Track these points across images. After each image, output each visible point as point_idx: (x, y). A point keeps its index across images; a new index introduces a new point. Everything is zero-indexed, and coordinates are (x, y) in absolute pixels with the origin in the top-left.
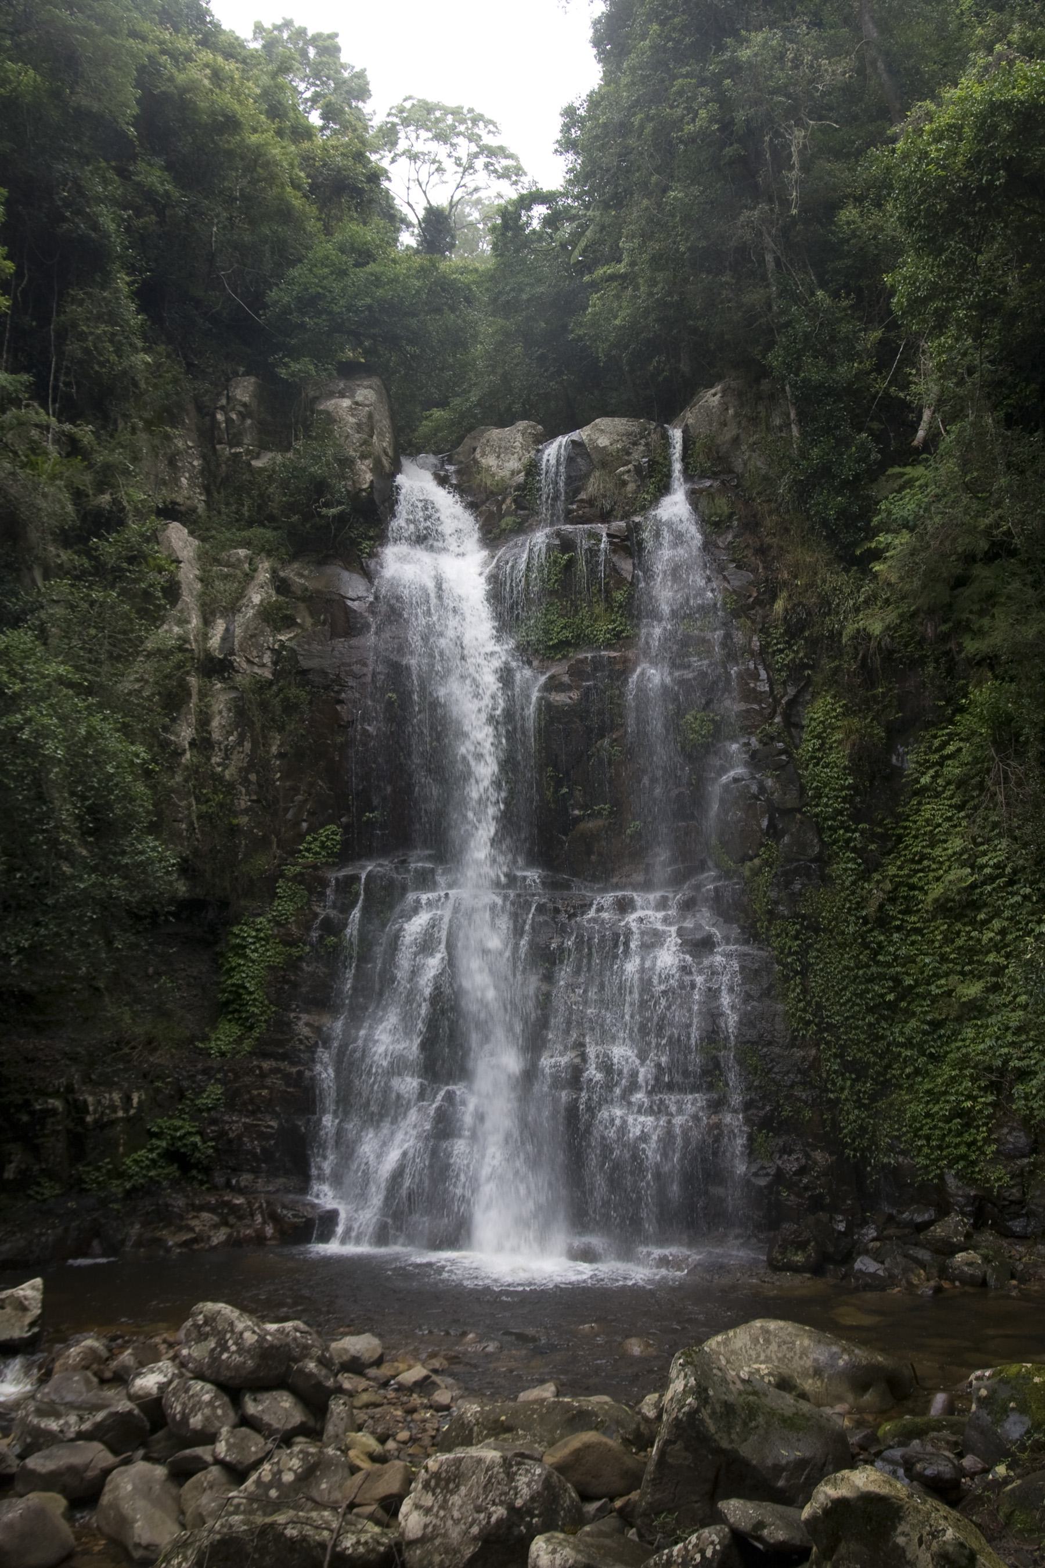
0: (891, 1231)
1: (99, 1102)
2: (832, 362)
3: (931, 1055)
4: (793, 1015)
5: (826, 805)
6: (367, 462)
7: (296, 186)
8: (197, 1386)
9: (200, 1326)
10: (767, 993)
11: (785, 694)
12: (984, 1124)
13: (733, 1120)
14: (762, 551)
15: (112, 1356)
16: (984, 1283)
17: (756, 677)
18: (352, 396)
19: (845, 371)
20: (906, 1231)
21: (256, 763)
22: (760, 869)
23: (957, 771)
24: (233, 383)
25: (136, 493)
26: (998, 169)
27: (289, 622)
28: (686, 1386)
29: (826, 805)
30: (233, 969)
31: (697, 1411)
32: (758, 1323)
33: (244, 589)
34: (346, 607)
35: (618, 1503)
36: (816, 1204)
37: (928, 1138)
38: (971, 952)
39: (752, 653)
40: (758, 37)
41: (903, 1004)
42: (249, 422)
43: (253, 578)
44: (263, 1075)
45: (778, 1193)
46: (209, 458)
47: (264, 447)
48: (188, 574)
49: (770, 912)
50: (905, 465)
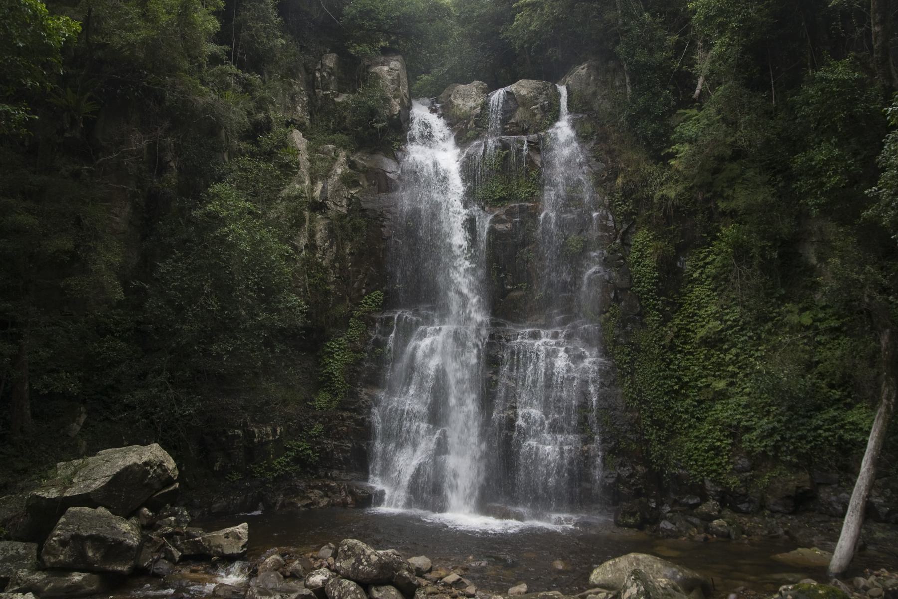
0: (677, 508)
2: (651, 51)
3: (698, 418)
5: (643, 287)
8: (346, 582)
10: (612, 384)
13: (595, 447)
14: (610, 152)
16: (728, 536)
17: (607, 219)
18: (388, 65)
19: (659, 56)
25: (277, 115)
27: (355, 184)
28: (638, 590)
32: (632, 555)
33: (332, 166)
36: (638, 493)
37: (696, 460)
38: (719, 365)
39: (605, 206)
41: (683, 391)
44: (343, 420)
46: (312, 96)
48: (304, 158)
49: (615, 342)
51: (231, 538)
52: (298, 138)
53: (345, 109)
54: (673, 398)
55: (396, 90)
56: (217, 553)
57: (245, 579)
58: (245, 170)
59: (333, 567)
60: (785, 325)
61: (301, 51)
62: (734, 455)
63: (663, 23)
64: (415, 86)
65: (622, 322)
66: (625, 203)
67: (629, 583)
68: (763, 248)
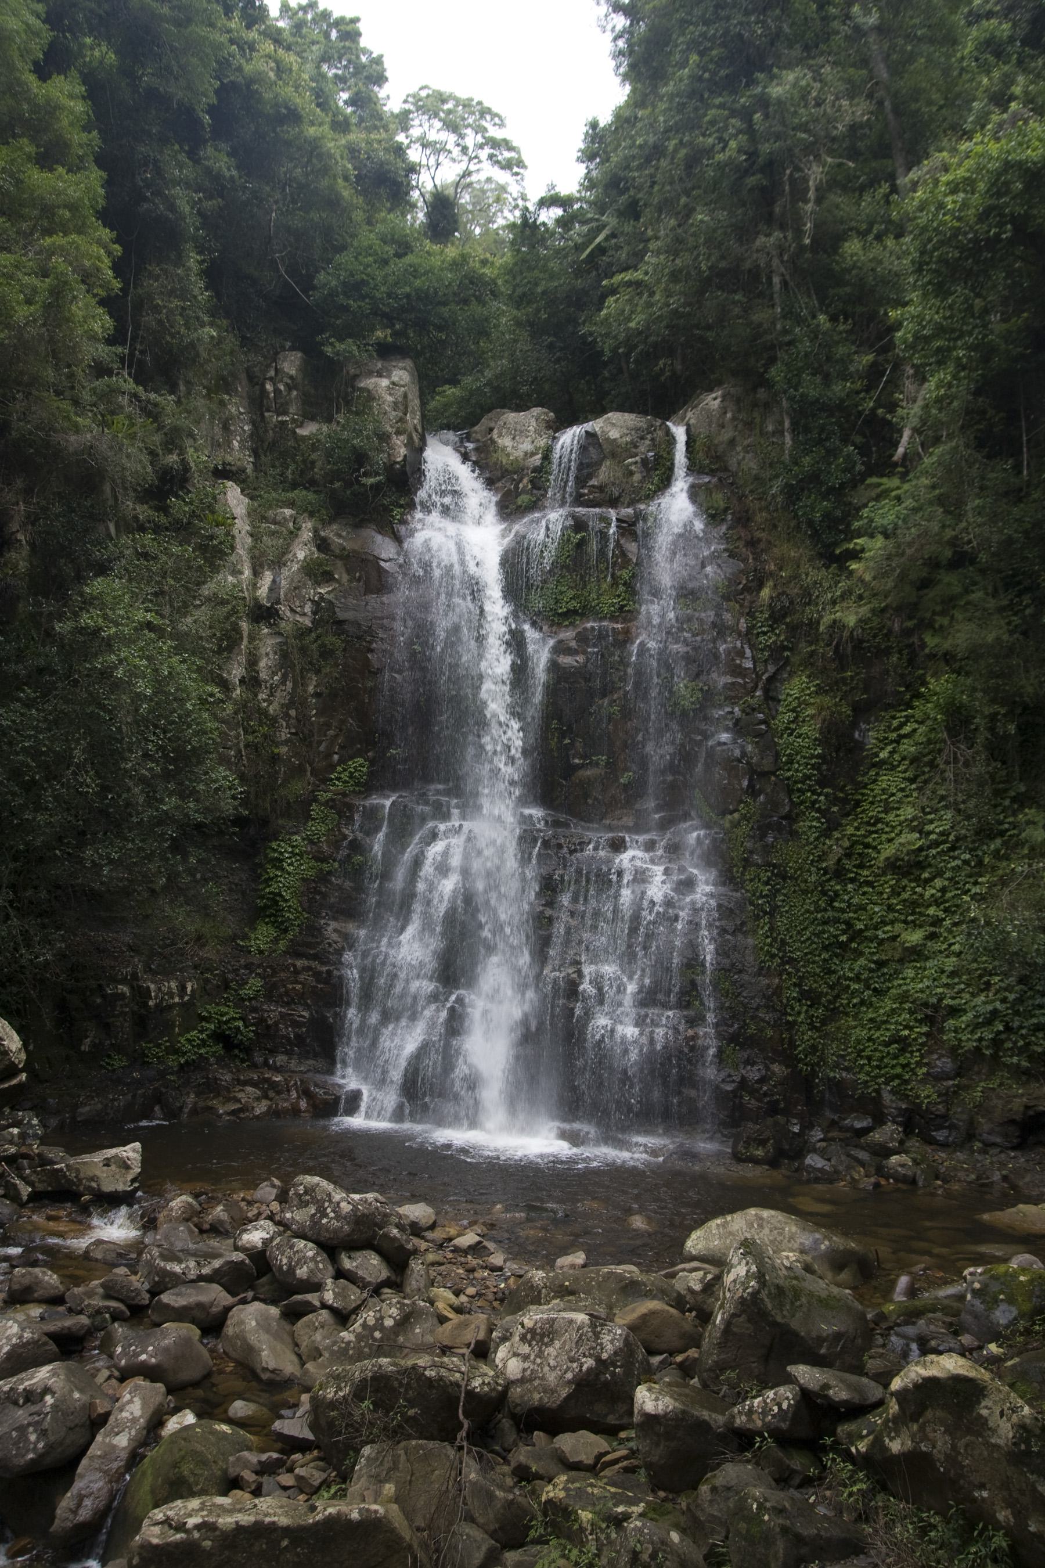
1: (160, 989)
2: (827, 379)
3: (875, 990)
4: (762, 949)
5: (797, 771)
6: (402, 438)
7: (346, 178)
8: (301, 1244)
9: (301, 1195)
11: (766, 671)
12: (919, 1050)
14: (752, 543)
15: (203, 1211)
16: (913, 1181)
17: (741, 654)
18: (389, 377)
19: (839, 389)
20: (848, 1135)
21: (295, 701)
22: (739, 822)
23: (913, 749)
24: (281, 356)
25: (198, 456)
26: (1006, 223)
27: (327, 577)
29: (797, 771)
30: (271, 879)
31: (758, 1292)
32: (752, 1211)
33: (289, 545)
34: (380, 567)
35: (679, 1359)
36: (773, 1109)
38: (913, 905)
39: (739, 634)
40: (791, 77)
41: (854, 945)
42: (295, 393)
43: (297, 536)
44: (296, 972)
45: (741, 1097)
46: (258, 424)
47: (310, 416)
48: (242, 527)
49: (746, 860)
50: (882, 476)
51: (113, 1167)
52: (235, 498)
53: (314, 448)
54: (837, 956)
55: (401, 420)
56: (90, 1189)
57: (138, 1233)
58: (145, 556)
59: (277, 1218)
60: (1023, 844)
61: (242, 347)
62: (931, 1052)
63: (849, 332)
64: (433, 404)
65: (759, 828)
66: (773, 630)
67: (735, 1261)
68: (993, 717)
